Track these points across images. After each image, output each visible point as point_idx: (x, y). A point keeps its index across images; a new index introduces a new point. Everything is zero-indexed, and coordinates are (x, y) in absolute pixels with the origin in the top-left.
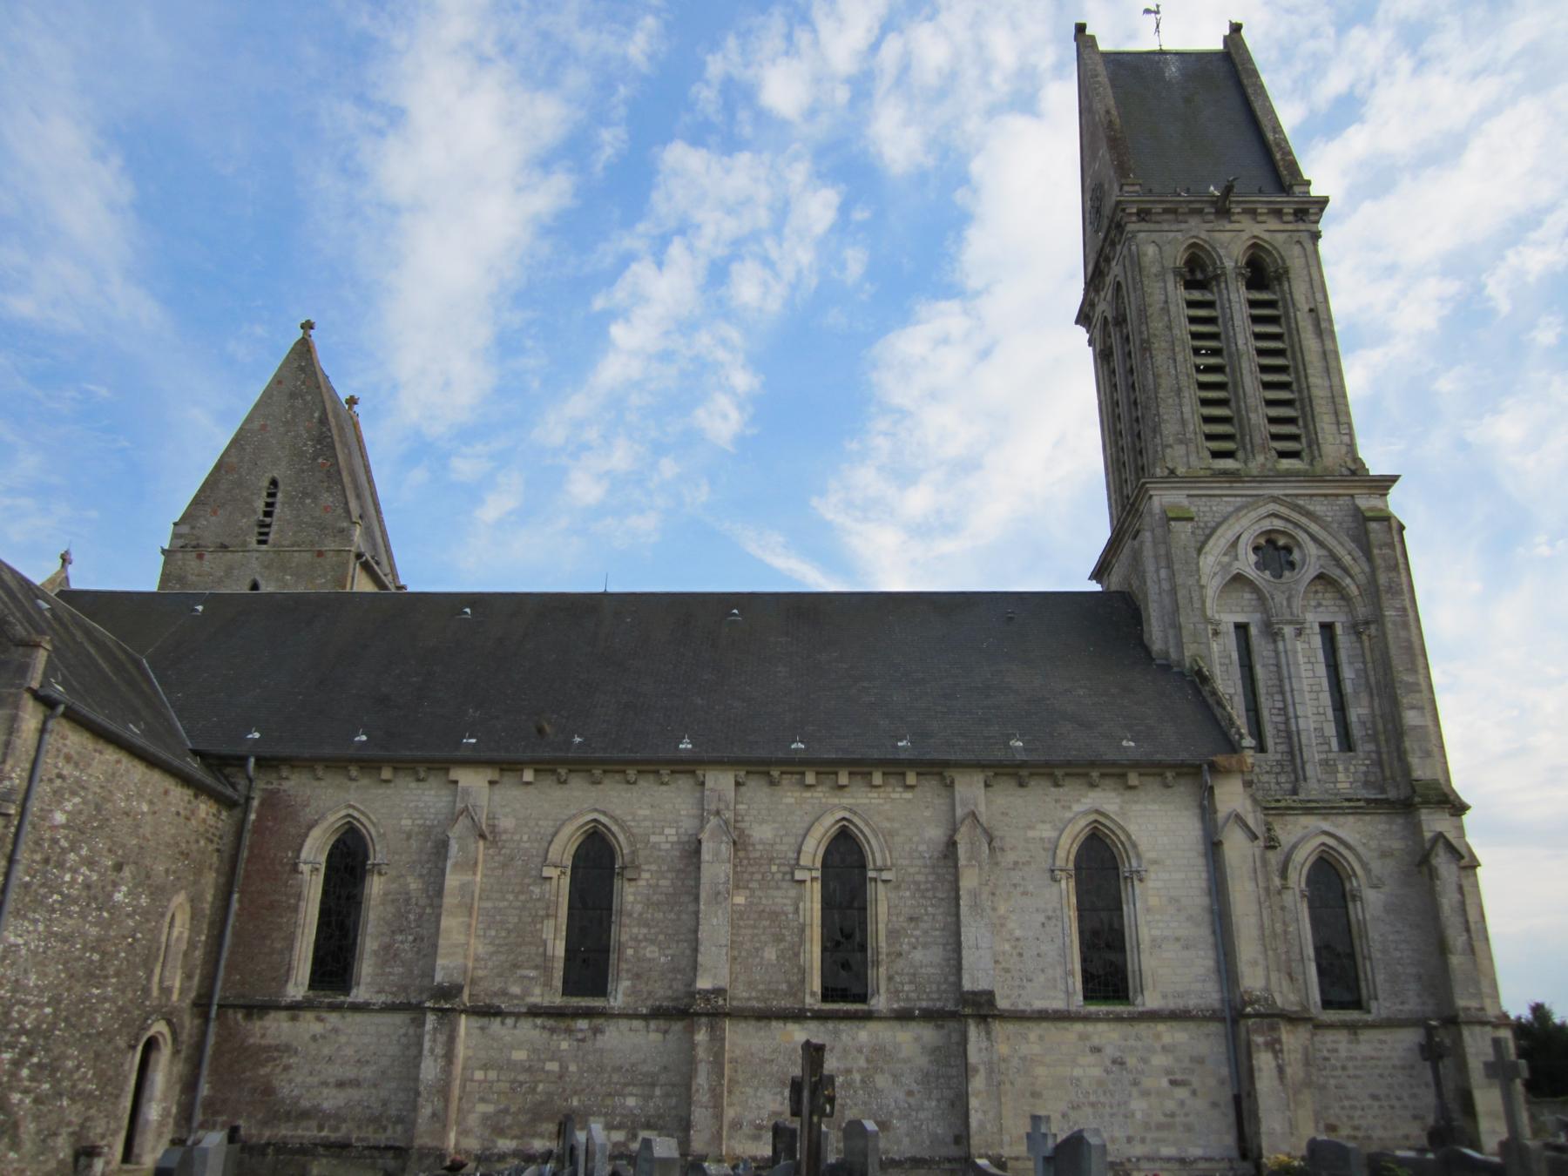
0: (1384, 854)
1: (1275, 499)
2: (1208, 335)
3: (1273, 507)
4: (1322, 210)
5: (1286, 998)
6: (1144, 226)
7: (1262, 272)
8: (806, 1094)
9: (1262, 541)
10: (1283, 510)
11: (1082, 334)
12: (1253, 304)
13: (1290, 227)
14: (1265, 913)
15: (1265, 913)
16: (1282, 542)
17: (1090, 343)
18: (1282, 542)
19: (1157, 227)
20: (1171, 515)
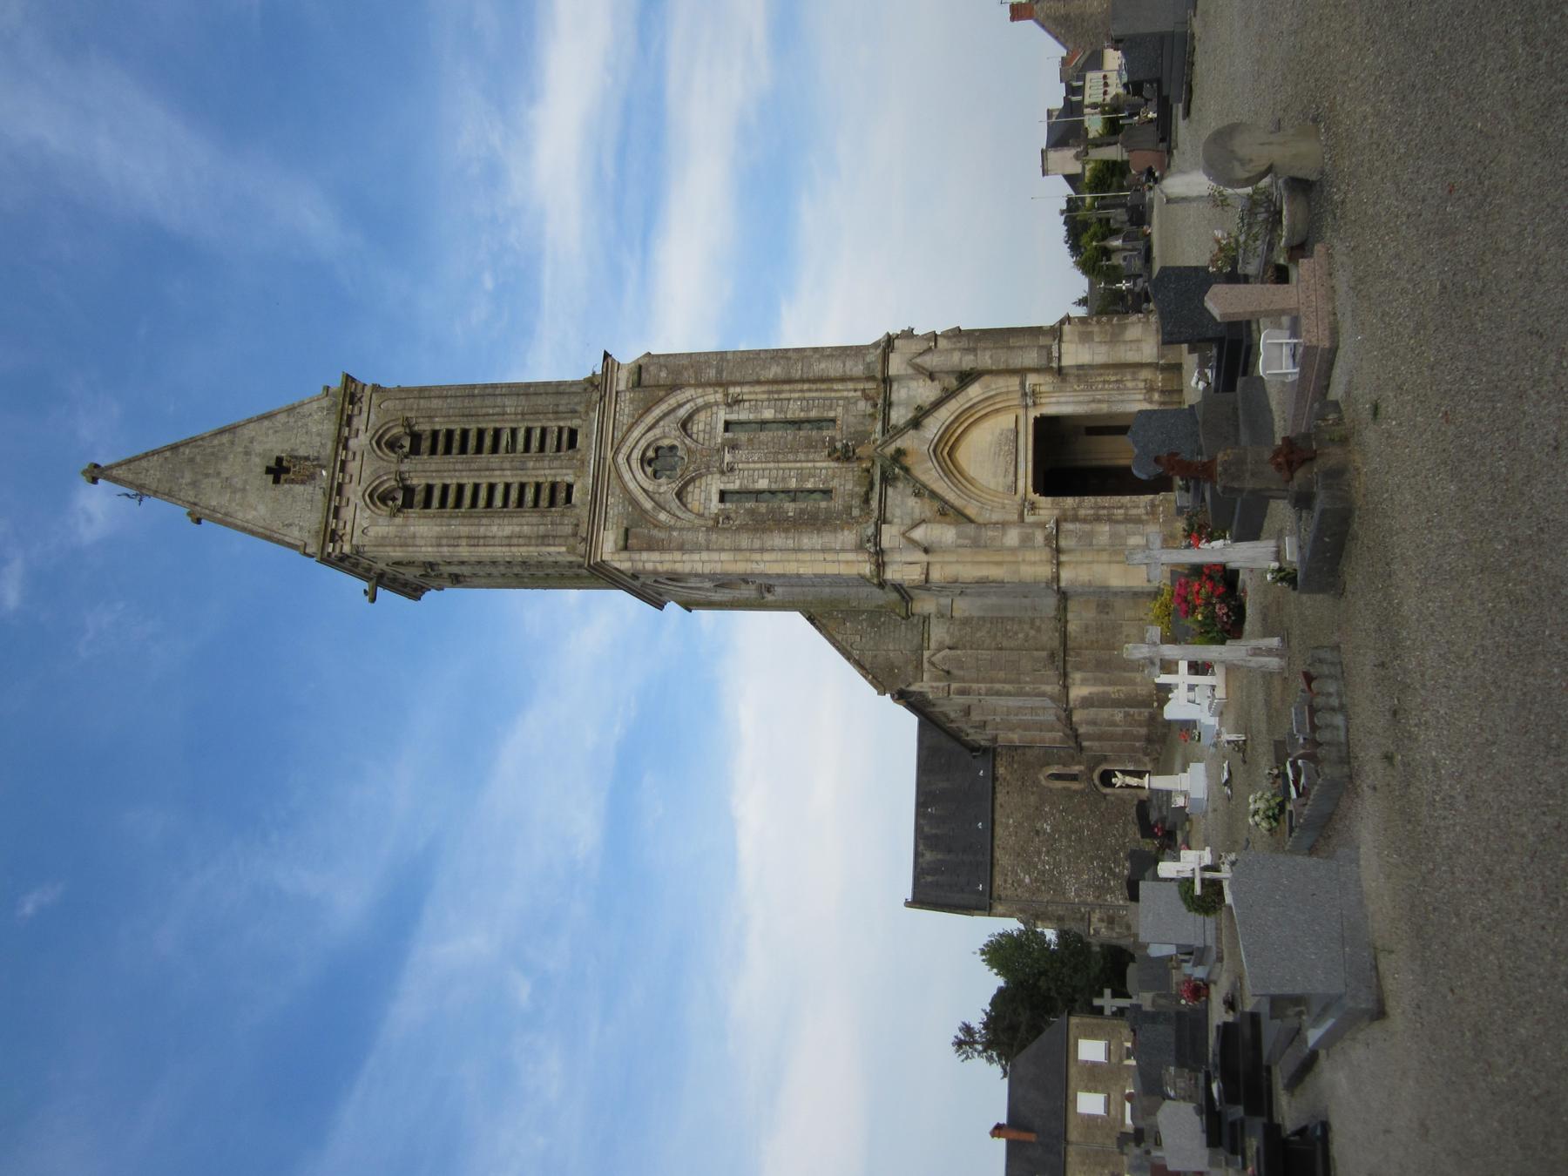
0: (967, 711)
1: (616, 453)
2: (449, 499)
3: (621, 459)
4: (353, 380)
5: (902, 372)
6: (347, 537)
7: (416, 442)
8: (998, 686)
9: (649, 470)
10: (625, 450)
11: (430, 596)
12: (433, 451)
13: (365, 409)
14: (1056, 354)
15: (1056, 354)
16: (651, 454)
17: (440, 588)
18: (651, 454)
19: (348, 528)
20: (621, 543)
